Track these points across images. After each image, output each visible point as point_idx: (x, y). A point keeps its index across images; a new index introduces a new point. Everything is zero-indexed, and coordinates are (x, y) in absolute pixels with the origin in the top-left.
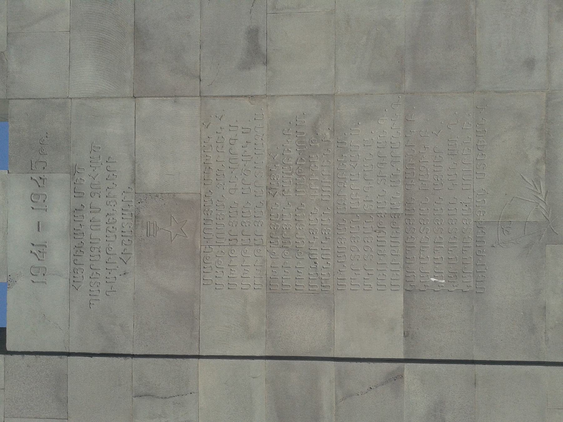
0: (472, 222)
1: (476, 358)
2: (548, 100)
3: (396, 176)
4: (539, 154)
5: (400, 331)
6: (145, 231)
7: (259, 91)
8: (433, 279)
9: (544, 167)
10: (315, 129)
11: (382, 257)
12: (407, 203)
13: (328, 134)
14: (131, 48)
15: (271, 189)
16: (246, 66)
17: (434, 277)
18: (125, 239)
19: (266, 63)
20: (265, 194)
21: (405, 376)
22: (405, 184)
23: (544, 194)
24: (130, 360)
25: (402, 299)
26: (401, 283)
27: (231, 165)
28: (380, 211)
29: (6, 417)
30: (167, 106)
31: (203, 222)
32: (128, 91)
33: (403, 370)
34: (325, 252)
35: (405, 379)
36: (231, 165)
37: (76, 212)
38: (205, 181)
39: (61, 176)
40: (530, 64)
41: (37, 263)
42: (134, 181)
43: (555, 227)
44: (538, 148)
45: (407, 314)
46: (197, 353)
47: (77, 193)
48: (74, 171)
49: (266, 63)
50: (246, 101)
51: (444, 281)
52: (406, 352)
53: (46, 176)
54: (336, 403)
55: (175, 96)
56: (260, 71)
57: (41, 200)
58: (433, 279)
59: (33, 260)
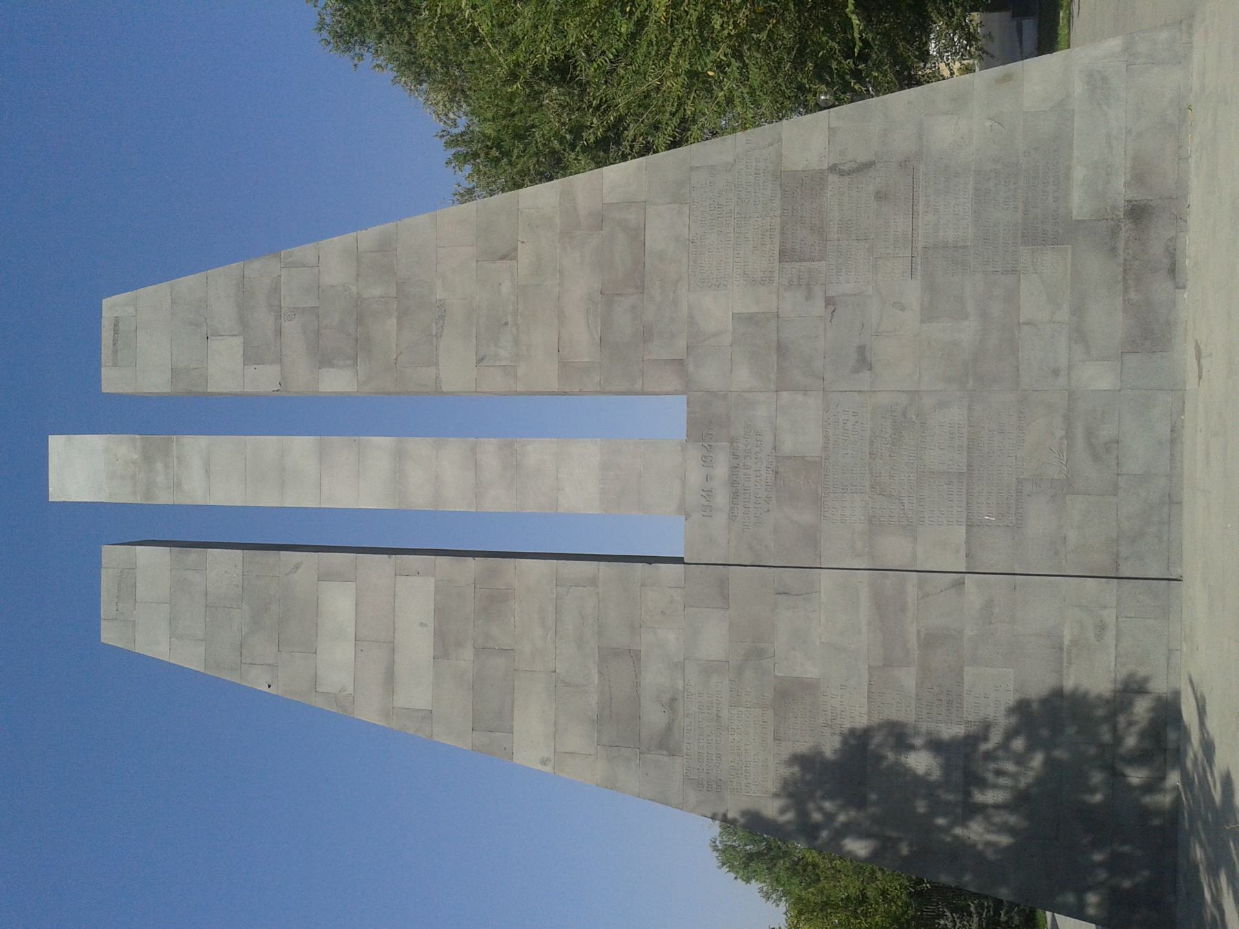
0: (1014, 479)
1: (1016, 572)
2: (1070, 396)
3: (962, 446)
4: (1063, 433)
5: (963, 553)
6: (782, 482)
7: (866, 388)
8: (987, 518)
9: (1066, 442)
10: (904, 414)
11: (950, 502)
12: (969, 465)
13: (914, 417)
14: (775, 358)
15: (873, 454)
16: (856, 371)
17: (988, 516)
18: (768, 487)
19: (870, 369)
20: (868, 457)
21: (966, 582)
22: (968, 452)
23: (1065, 460)
24: (773, 569)
25: (965, 531)
26: (964, 520)
27: (844, 438)
28: (950, 470)
29: (400, 575)
30: (799, 397)
31: (823, 476)
32: (773, 386)
33: (964, 578)
34: (911, 498)
35: (966, 585)
36: (844, 438)
37: (734, 468)
38: (825, 448)
39: (724, 444)
40: (1056, 372)
41: (706, 503)
42: (775, 448)
43: (405, 85)
44: (1062, 429)
45: (968, 542)
46: (819, 566)
47: (735, 456)
48: (732, 441)
49: (870, 369)
50: (856, 394)
51: (994, 519)
52: (967, 568)
53: (713, 444)
54: (918, 600)
55: (805, 391)
56: (866, 375)
57: (709, 460)
58: (987, 518)
59: (704, 502)
